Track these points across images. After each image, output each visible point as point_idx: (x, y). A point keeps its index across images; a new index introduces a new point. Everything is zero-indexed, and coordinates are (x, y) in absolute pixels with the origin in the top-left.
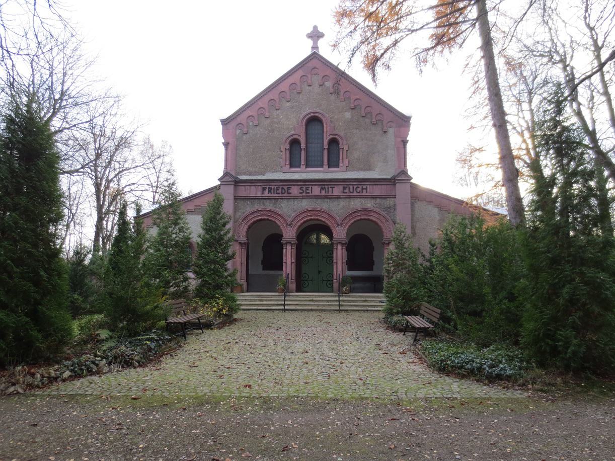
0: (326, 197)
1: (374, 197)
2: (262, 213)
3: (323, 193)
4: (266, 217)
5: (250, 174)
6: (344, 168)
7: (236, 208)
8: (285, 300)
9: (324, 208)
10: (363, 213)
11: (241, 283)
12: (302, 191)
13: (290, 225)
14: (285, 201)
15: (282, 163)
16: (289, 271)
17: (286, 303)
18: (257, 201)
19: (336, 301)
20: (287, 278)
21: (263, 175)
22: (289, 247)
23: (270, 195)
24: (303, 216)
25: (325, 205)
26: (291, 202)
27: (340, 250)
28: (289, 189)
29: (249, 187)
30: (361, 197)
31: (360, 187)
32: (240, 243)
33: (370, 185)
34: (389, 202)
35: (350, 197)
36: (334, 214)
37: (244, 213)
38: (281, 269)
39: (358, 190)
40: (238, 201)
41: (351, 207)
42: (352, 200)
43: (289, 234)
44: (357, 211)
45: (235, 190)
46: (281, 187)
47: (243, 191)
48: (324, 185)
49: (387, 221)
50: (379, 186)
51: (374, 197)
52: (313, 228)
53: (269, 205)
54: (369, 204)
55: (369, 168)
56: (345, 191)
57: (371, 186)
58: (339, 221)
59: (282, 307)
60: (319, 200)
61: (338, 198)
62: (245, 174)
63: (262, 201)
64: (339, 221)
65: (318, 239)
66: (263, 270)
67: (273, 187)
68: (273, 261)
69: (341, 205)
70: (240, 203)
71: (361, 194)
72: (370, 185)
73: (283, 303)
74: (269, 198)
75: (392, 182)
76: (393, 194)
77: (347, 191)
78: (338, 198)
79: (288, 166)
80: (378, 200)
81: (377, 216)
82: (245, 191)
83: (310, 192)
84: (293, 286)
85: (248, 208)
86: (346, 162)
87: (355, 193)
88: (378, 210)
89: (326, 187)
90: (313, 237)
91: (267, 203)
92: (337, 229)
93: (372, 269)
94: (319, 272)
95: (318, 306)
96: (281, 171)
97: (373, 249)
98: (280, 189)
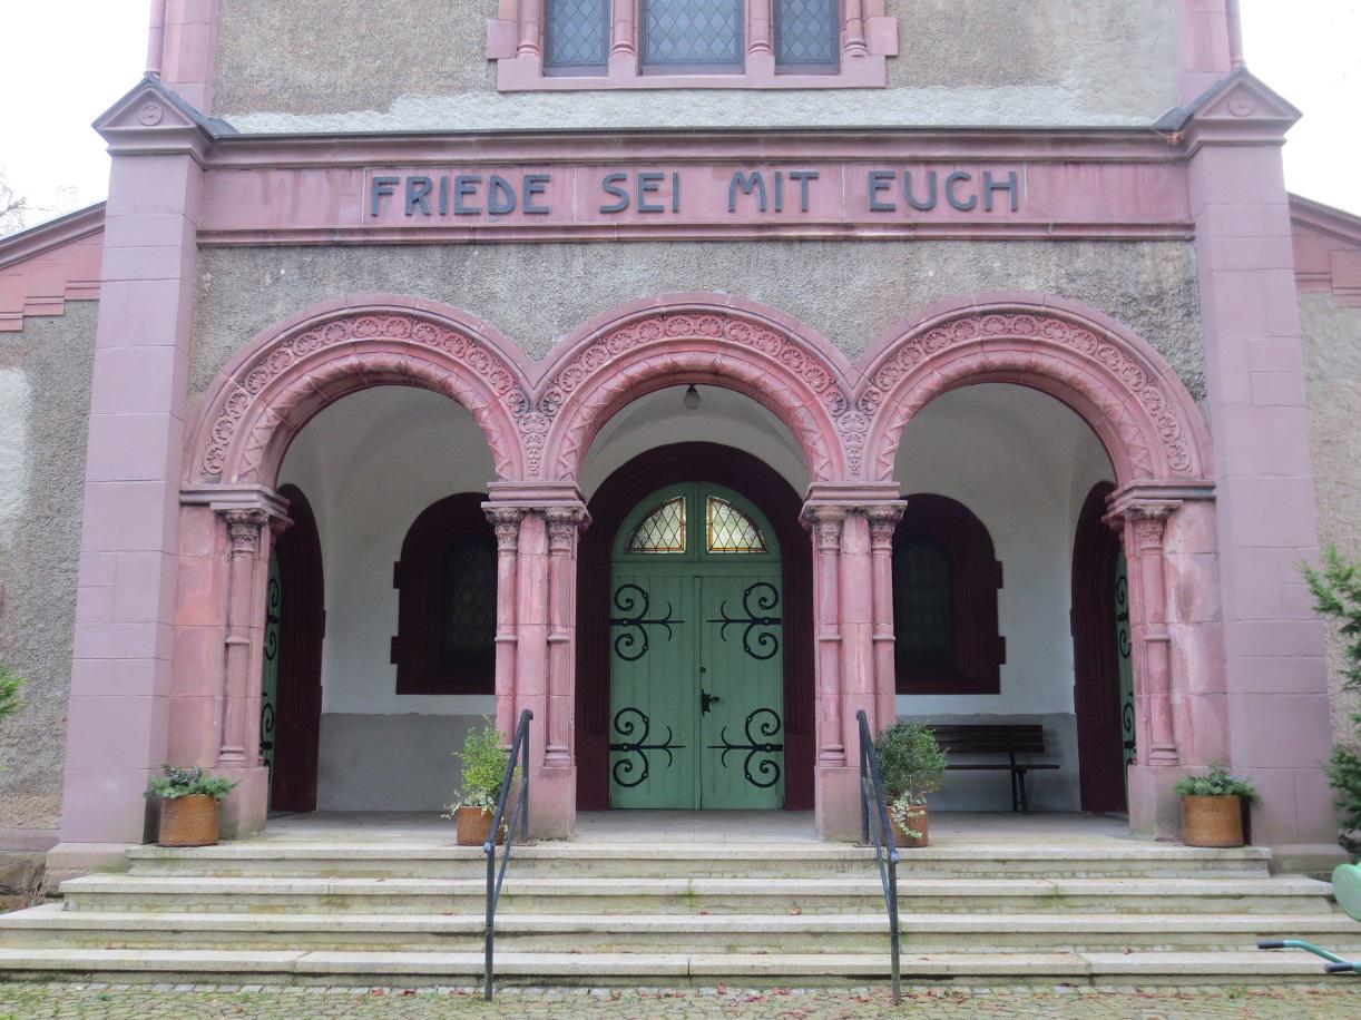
0: (767, 235)
1: (1064, 236)
2: (369, 331)
3: (749, 210)
4: (391, 359)
5: (302, 102)
6: (872, 69)
7: (200, 308)
8: (492, 898)
9: (755, 296)
10: (995, 329)
11: (211, 779)
12: (613, 202)
13: (544, 403)
14: (510, 259)
15: (497, 42)
16: (530, 698)
17: (504, 919)
18: (336, 259)
19: (857, 900)
20: (521, 734)
21: (382, 108)
22: (533, 542)
23: (416, 221)
24: (623, 345)
25: (750, 282)
26: (551, 261)
27: (863, 561)
28: (534, 187)
29: (287, 177)
30: (983, 234)
31: (976, 173)
32: (221, 514)
33: (1033, 162)
34: (1155, 266)
35: (914, 235)
36: (813, 336)
37: (252, 332)
38: (487, 687)
39: (964, 193)
40: (223, 260)
41: (924, 292)
42: (925, 250)
43: (537, 463)
44: (961, 319)
45: (203, 197)
46: (486, 175)
47: (251, 202)
48: (751, 162)
49: (1151, 380)
50: (1085, 173)
51: (1064, 236)
52: (687, 456)
53: (410, 283)
54: (1032, 277)
55: (1022, 69)
56: (884, 198)
57: (1040, 173)
58: (852, 383)
59: (470, 958)
60: (724, 253)
61: (843, 236)
62: (269, 103)
63: (367, 258)
64: (852, 383)
65: (696, 528)
66: (402, 688)
67: (435, 176)
68: (446, 640)
69: (860, 282)
70: (234, 270)
71: (977, 216)
72: (1033, 162)
73: (477, 920)
74: (410, 242)
75: (1173, 144)
76: (1179, 216)
77: (891, 197)
78: (843, 236)
79: (533, 59)
80: (1087, 250)
81: (1081, 346)
82: (266, 200)
83: (666, 203)
84: (556, 790)
85: (280, 300)
86: (884, 34)
87: (943, 213)
88: (1093, 313)
89: (766, 174)
90: (667, 532)
91: (401, 268)
92: (837, 425)
93: (991, 686)
94: (706, 702)
95: (731, 940)
96: (491, 87)
97: (993, 575)
98: (484, 190)
